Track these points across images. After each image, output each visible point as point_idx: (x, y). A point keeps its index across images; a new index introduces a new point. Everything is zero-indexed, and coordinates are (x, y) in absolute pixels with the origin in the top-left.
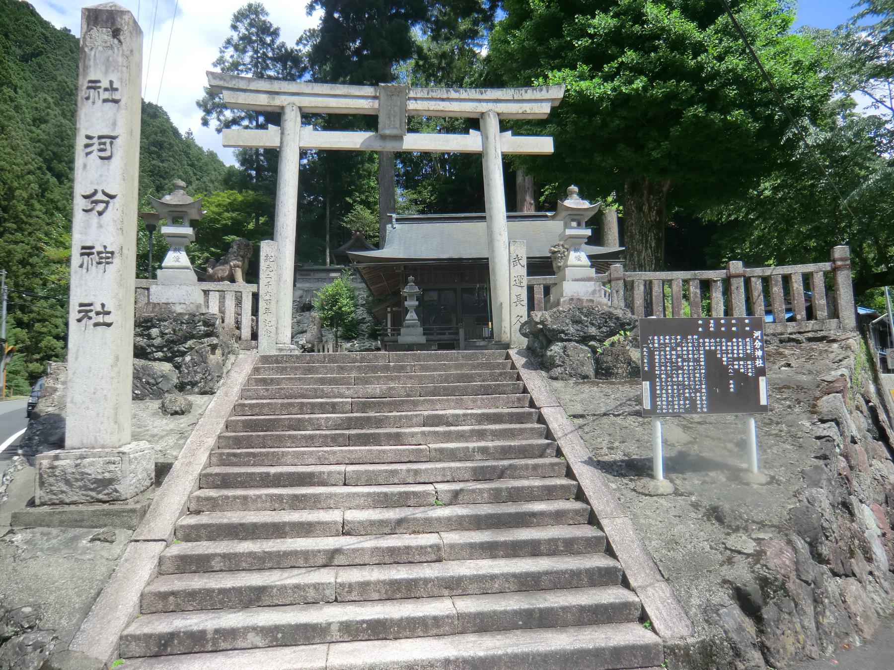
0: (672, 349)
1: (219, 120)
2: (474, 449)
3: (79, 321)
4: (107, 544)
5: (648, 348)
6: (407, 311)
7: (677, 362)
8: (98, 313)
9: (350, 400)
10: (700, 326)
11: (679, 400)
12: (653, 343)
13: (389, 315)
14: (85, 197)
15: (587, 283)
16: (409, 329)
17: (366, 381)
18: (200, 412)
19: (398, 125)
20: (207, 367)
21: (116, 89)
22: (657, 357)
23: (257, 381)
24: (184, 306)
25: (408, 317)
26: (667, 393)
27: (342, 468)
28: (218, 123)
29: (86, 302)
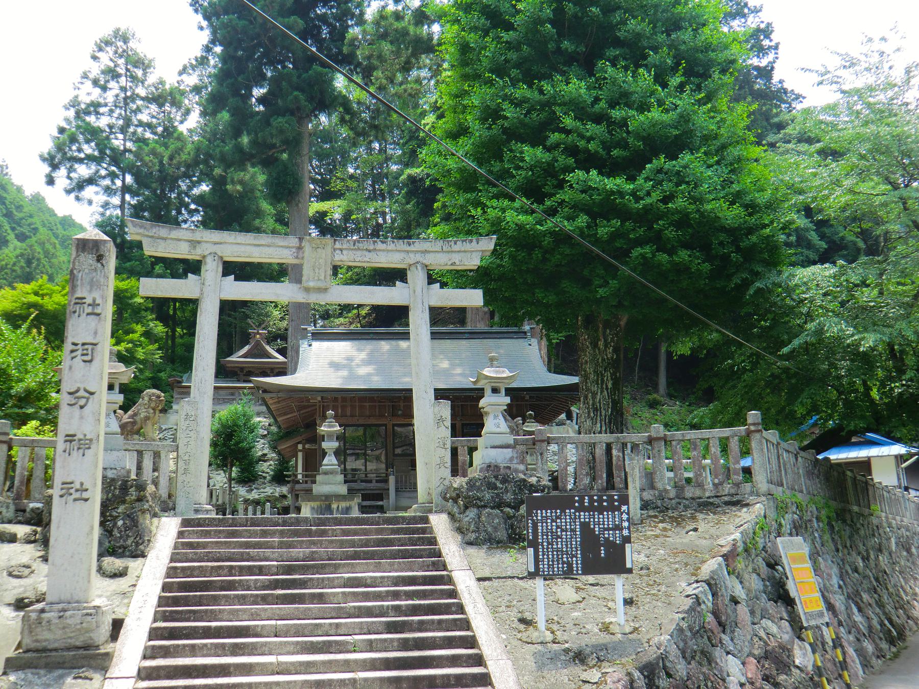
0: (553, 521)
1: (69, 177)
2: (388, 606)
3: (61, 496)
4: (88, 681)
5: (533, 520)
6: (324, 454)
7: (557, 532)
8: (77, 490)
9: (275, 563)
10: (576, 501)
11: (558, 564)
12: (537, 516)
13: (300, 455)
14: (70, 393)
15: (505, 450)
16: (327, 477)
17: (290, 546)
18: (136, 574)
19: (322, 277)
20: (138, 531)
21: (99, 305)
22: (540, 528)
23: (183, 544)
24: (115, 471)
25: (325, 462)
26: (548, 558)
27: (273, 622)
28: (68, 181)
29: (69, 480)
